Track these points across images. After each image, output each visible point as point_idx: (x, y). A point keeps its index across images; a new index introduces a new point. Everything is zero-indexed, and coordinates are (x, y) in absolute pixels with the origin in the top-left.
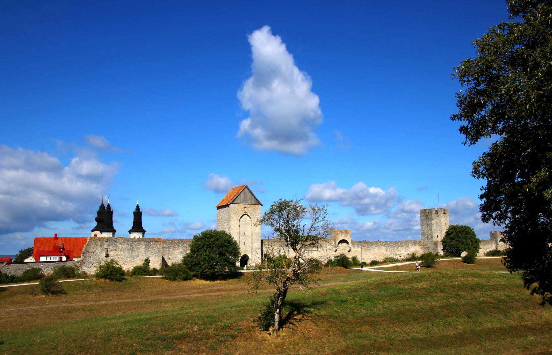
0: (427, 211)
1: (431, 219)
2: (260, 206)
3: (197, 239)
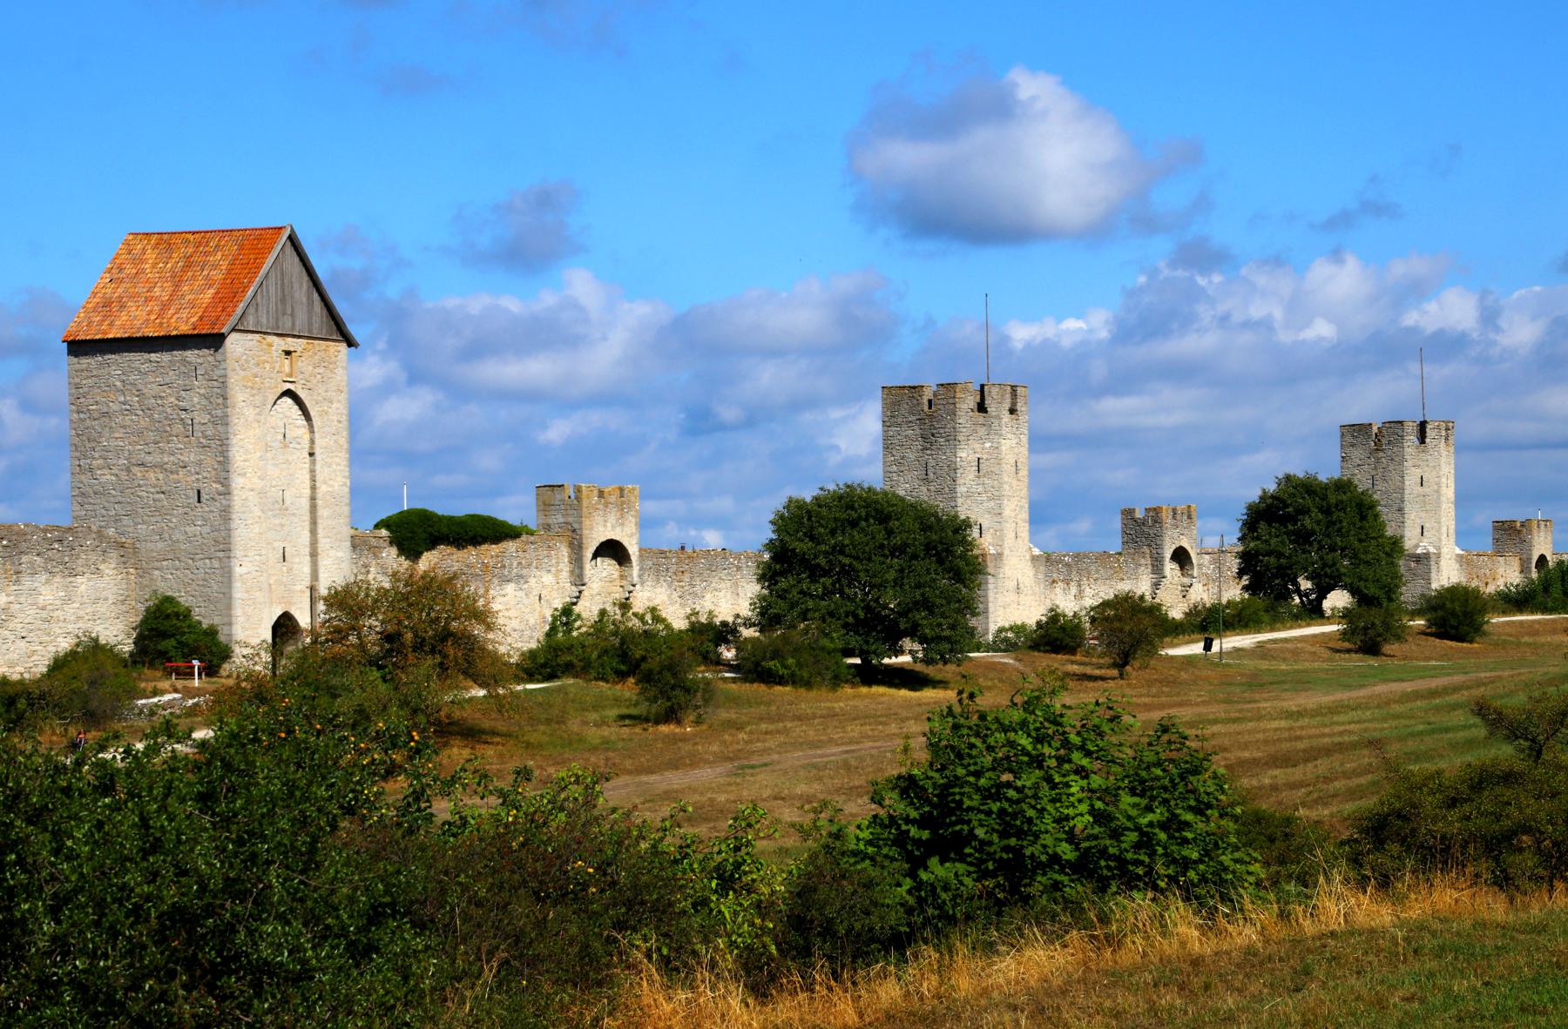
0: (928, 394)
1: (952, 439)
2: (343, 347)
3: (961, 527)
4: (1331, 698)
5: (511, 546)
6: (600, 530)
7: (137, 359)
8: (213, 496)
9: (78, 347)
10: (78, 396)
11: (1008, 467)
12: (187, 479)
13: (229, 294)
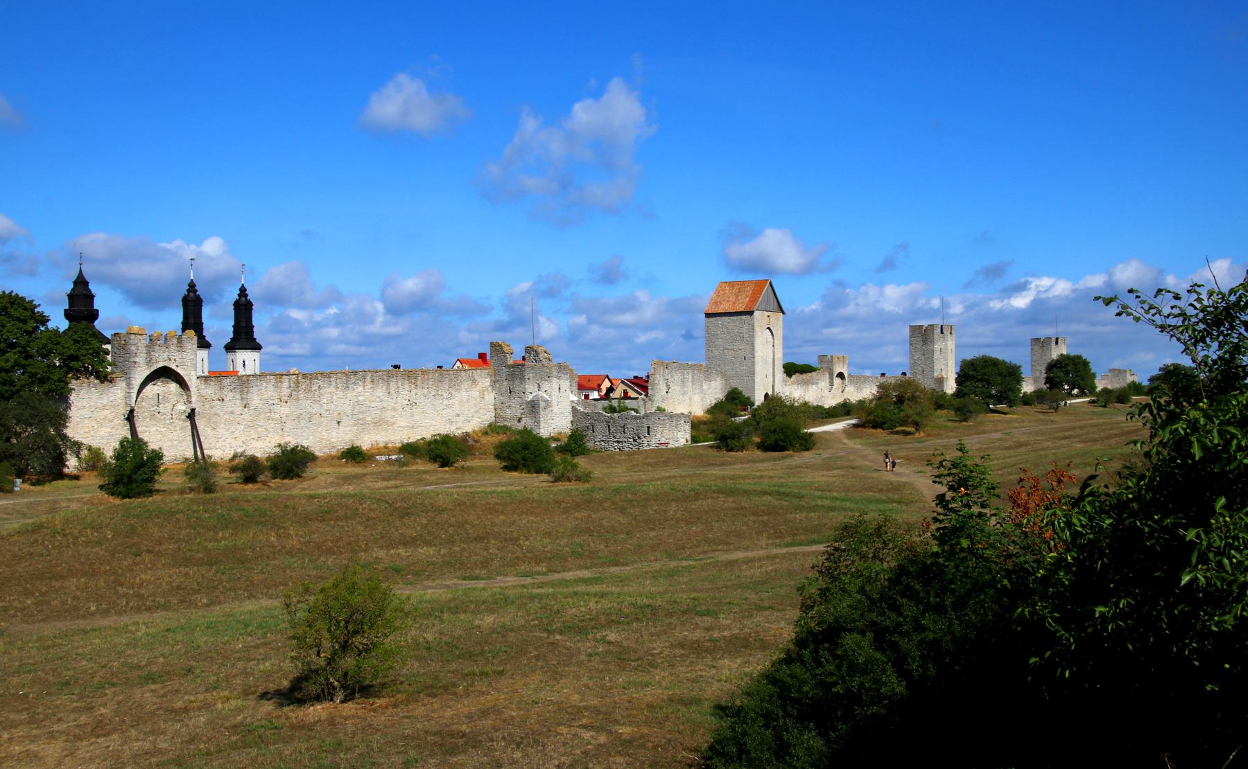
1: (933, 342)
4: (728, 471)
5: (814, 374)
6: (837, 370)
7: (726, 318)
8: (750, 358)
9: (708, 315)
10: (708, 330)
12: (741, 354)
13: (754, 299)
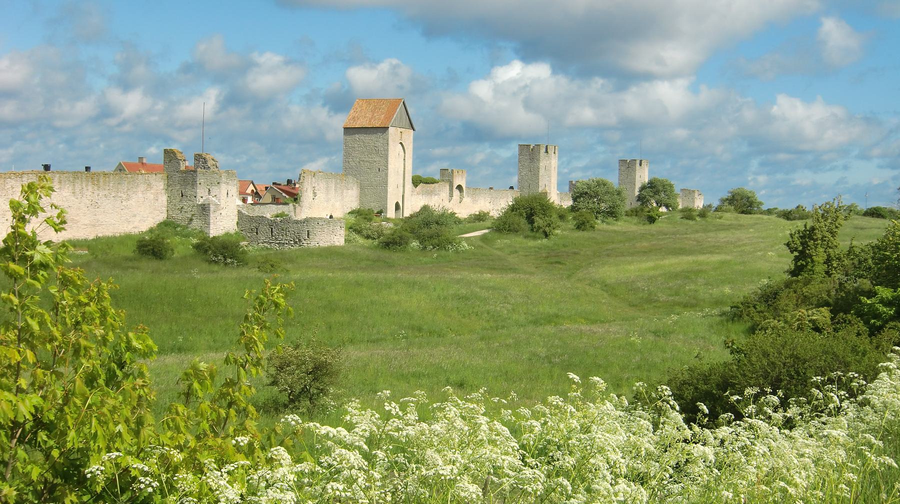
11: (553, 168)
